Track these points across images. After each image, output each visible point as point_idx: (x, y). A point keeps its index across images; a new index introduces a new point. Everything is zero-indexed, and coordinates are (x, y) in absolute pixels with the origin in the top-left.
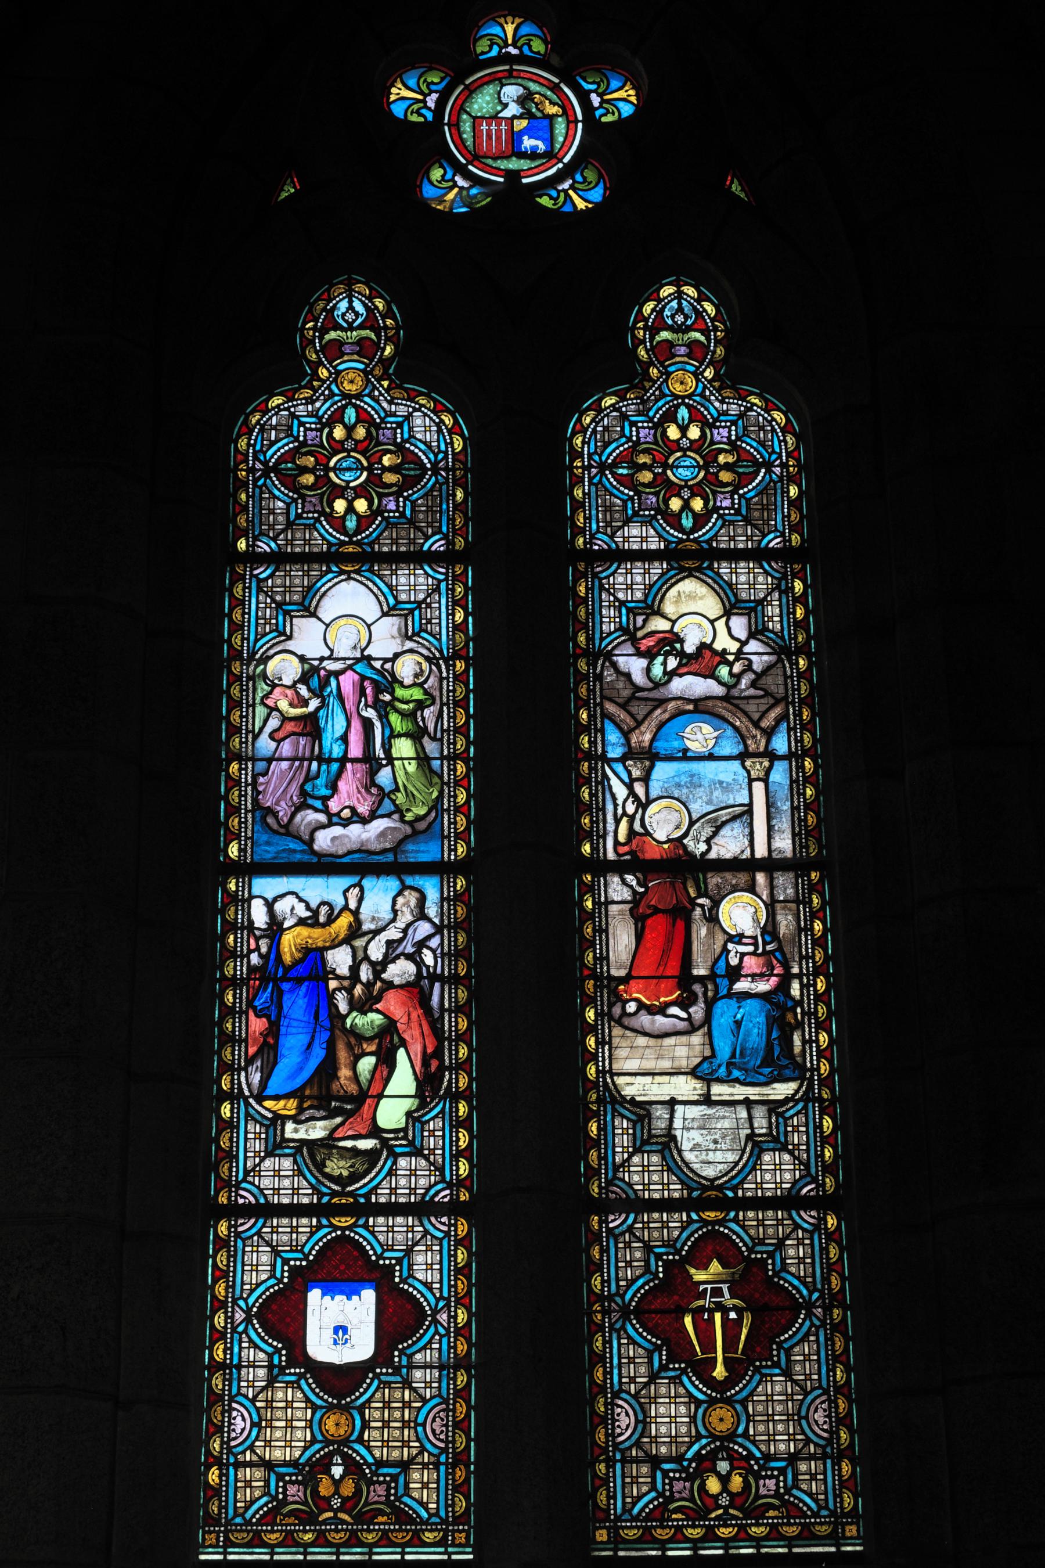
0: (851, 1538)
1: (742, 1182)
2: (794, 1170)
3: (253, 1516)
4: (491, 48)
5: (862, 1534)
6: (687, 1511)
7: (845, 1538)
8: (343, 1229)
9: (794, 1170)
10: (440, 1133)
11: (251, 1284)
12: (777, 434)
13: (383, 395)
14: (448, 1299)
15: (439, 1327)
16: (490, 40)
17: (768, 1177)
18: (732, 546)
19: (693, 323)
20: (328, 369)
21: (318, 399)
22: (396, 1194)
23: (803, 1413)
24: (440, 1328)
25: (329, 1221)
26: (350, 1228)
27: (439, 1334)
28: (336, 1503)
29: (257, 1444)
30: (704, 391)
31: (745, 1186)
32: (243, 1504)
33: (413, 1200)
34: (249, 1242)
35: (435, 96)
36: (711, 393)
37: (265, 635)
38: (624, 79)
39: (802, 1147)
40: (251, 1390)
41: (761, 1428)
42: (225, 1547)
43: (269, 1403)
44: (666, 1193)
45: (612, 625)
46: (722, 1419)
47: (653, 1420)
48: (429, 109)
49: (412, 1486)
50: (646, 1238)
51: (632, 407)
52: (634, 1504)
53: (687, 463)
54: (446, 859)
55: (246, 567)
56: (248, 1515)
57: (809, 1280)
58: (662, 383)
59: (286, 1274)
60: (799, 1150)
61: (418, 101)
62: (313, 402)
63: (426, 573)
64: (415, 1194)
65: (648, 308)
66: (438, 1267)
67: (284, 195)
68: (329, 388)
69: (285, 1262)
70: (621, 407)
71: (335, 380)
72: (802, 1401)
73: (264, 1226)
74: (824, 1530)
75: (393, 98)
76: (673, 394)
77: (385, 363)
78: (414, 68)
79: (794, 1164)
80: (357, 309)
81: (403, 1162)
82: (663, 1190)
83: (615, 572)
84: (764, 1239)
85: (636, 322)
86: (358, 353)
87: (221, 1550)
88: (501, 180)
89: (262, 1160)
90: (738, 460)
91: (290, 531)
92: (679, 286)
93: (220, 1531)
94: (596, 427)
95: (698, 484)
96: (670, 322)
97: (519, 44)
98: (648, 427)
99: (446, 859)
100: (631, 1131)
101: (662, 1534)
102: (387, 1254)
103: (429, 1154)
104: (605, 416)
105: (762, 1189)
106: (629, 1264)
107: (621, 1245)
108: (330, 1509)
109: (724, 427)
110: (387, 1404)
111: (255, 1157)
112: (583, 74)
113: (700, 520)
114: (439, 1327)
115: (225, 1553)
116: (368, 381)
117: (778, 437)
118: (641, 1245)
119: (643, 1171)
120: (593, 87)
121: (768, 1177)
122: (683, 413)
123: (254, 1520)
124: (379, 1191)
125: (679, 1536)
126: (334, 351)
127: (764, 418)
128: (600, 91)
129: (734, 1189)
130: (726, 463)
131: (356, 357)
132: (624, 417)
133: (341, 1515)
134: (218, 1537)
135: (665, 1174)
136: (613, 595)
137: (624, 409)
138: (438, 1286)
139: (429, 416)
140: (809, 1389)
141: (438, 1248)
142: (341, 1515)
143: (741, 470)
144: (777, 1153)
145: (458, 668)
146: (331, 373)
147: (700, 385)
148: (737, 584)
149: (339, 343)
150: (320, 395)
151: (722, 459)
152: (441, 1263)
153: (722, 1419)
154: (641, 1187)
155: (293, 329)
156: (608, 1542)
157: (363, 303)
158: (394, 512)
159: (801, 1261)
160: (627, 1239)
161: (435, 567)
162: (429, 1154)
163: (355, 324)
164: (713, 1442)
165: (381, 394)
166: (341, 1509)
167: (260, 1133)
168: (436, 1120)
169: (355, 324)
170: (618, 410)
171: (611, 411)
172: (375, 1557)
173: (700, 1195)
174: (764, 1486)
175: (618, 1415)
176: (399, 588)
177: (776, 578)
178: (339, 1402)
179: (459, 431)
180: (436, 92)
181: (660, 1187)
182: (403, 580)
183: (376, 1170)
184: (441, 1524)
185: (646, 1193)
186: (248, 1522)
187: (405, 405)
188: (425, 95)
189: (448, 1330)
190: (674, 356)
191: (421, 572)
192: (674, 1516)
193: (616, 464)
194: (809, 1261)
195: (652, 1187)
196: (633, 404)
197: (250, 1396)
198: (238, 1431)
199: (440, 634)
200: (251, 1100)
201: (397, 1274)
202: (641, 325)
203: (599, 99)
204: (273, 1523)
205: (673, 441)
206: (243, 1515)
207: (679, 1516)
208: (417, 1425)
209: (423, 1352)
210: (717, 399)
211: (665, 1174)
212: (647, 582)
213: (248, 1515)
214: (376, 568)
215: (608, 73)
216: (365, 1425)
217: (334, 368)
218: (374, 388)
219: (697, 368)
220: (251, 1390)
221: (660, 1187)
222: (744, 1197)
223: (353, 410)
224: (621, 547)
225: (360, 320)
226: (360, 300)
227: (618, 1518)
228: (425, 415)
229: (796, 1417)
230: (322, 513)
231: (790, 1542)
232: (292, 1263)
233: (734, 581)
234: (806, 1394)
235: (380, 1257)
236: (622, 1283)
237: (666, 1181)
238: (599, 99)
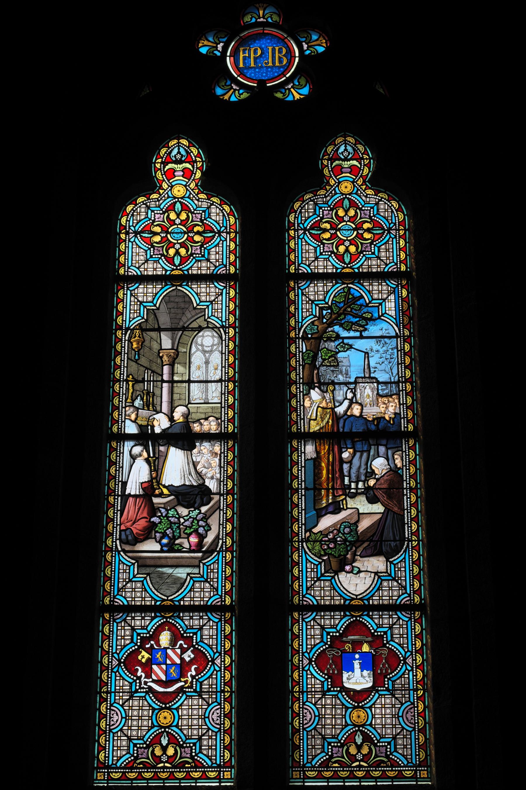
0: (424, 778)
1: (372, 596)
2: (211, 591)
3: (316, 764)
4: (251, 19)
5: (233, 777)
6: (341, 763)
7: (97, 779)
8: (356, 617)
9: (211, 591)
10: (120, 571)
11: (121, 646)
12: (225, 217)
13: (362, 193)
14: (412, 652)
15: (408, 666)
16: (251, 15)
17: (386, 593)
18: (199, 273)
19: (185, 159)
20: (334, 180)
21: (328, 195)
22: (145, 600)
23: (400, 714)
24: (408, 666)
25: (350, 613)
26: (360, 616)
27: (408, 670)
28: (164, 758)
29: (124, 728)
30: (190, 195)
31: (374, 598)
32: (311, 757)
33: (202, 604)
34: (119, 625)
35: (222, 44)
36: (194, 196)
37: (134, 318)
38: (319, 35)
39: (214, 580)
40: (121, 700)
41: (185, 722)
42: (304, 779)
43: (131, 708)
44: (391, 601)
45: (135, 314)
46: (165, 717)
47: (130, 718)
48: (219, 51)
49: (398, 747)
50: (322, 624)
51: (153, 203)
52: (118, 760)
53: (347, 228)
54: (223, 431)
55: (227, 283)
56: (313, 763)
57: (405, 646)
58: (335, 187)
59: (139, 641)
60: (213, 581)
61: (214, 47)
62: (326, 197)
63: (387, 284)
64: (203, 601)
65: (330, 149)
66: (405, 636)
67: (143, 94)
68: (334, 189)
69: (328, 633)
70: (147, 203)
71: (338, 186)
72: (206, 709)
73: (316, 615)
74: (212, 775)
75: (200, 45)
76: (341, 193)
77: (364, 178)
78: (211, 31)
79: (211, 589)
80: (182, 153)
81: (385, 584)
82: (142, 601)
83: (309, 286)
84: (193, 626)
85: (323, 156)
86: (183, 176)
87: (106, 782)
88: (256, 85)
89: (315, 582)
90: (373, 227)
91: (316, 262)
92: (345, 138)
93: (105, 772)
94: (301, 210)
95: (353, 239)
96: (174, 159)
97: (266, 17)
98: (160, 213)
99: (223, 431)
100: (315, 570)
101: (328, 774)
102: (379, 630)
103: (210, 581)
104: (306, 204)
105: (135, 601)
106: (123, 637)
107: (119, 628)
108: (357, 760)
109: (198, 214)
110: (191, 707)
111: (311, 581)
112: (299, 33)
113: (184, 260)
114: (408, 666)
115: (304, 782)
116: (187, 190)
117: (395, 215)
118: (319, 627)
119: (389, 590)
120: (304, 39)
121: (386, 593)
122: (178, 206)
123: (317, 765)
124: (374, 598)
125: (172, 777)
126: (339, 170)
127: (388, 205)
128: (307, 41)
129: (368, 600)
130: (198, 231)
131: (348, 175)
132: (148, 208)
133: (362, 763)
134: (104, 775)
135: (143, 592)
136: (308, 298)
137: (148, 204)
138: (215, 647)
139: (387, 204)
140: (210, 703)
141: (405, 626)
142: (362, 763)
143: (375, 232)
144: (390, 582)
145: (294, 333)
146: (336, 182)
147: (356, 189)
148: (372, 291)
149: (173, 171)
150: (330, 194)
151: (196, 229)
152: (217, 635)
153: (165, 717)
154: (130, 599)
155: (148, 164)
156: (428, 778)
157: (185, 149)
158: (199, 254)
159: (211, 637)
160: (312, 624)
161: (391, 281)
162: (210, 581)
163: (349, 157)
164: (355, 728)
165: (361, 193)
166: (362, 760)
167: (314, 568)
168: (215, 564)
169: (349, 157)
170: (146, 204)
171: (309, 202)
172: (306, 784)
173: (161, 603)
174: (185, 751)
175: (306, 713)
176: (373, 292)
177: (393, 288)
178: (166, 706)
179: (232, 214)
180: (223, 42)
181: (388, 598)
182: (375, 288)
183: (183, 590)
184: (413, 767)
185: (133, 602)
186: (314, 767)
187: (374, 198)
188: (217, 44)
189: (412, 667)
190: (175, 176)
191: (213, 286)
192: (334, 765)
193: (143, 231)
194: (405, 636)
195: (195, 599)
196: (320, 198)
197: (121, 703)
198: (308, 719)
199: (222, 317)
200: (122, 553)
201: (385, 639)
202: (326, 157)
203: (306, 46)
204: (328, 767)
205: (341, 217)
206: (311, 763)
207: (337, 765)
208: (399, 717)
209: (208, 680)
210: (196, 199)
211: (143, 592)
212: (325, 290)
213: (313, 763)
214: (190, 284)
215: (310, 31)
216: (373, 716)
217: (338, 179)
218: (190, 193)
219: (187, 183)
220: (121, 700)
221: (388, 598)
222: (184, 605)
223: (179, 205)
224: (143, 273)
225: (350, 156)
226: (184, 148)
227: (304, 766)
228: (217, 207)
229: (321, 716)
230: (162, 255)
231: (328, 779)
232: (142, 635)
233: (371, 290)
234: (209, 705)
235: (149, 633)
236: (309, 647)
237: (143, 596)
238: (306, 46)
